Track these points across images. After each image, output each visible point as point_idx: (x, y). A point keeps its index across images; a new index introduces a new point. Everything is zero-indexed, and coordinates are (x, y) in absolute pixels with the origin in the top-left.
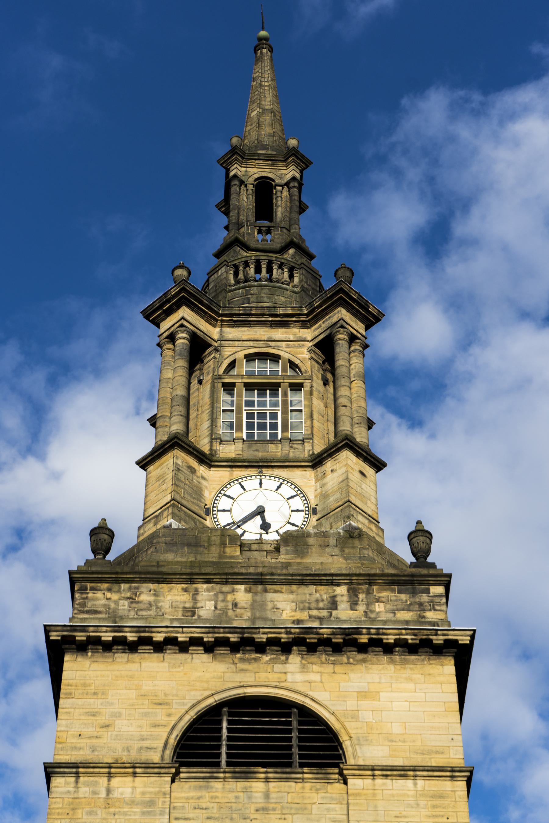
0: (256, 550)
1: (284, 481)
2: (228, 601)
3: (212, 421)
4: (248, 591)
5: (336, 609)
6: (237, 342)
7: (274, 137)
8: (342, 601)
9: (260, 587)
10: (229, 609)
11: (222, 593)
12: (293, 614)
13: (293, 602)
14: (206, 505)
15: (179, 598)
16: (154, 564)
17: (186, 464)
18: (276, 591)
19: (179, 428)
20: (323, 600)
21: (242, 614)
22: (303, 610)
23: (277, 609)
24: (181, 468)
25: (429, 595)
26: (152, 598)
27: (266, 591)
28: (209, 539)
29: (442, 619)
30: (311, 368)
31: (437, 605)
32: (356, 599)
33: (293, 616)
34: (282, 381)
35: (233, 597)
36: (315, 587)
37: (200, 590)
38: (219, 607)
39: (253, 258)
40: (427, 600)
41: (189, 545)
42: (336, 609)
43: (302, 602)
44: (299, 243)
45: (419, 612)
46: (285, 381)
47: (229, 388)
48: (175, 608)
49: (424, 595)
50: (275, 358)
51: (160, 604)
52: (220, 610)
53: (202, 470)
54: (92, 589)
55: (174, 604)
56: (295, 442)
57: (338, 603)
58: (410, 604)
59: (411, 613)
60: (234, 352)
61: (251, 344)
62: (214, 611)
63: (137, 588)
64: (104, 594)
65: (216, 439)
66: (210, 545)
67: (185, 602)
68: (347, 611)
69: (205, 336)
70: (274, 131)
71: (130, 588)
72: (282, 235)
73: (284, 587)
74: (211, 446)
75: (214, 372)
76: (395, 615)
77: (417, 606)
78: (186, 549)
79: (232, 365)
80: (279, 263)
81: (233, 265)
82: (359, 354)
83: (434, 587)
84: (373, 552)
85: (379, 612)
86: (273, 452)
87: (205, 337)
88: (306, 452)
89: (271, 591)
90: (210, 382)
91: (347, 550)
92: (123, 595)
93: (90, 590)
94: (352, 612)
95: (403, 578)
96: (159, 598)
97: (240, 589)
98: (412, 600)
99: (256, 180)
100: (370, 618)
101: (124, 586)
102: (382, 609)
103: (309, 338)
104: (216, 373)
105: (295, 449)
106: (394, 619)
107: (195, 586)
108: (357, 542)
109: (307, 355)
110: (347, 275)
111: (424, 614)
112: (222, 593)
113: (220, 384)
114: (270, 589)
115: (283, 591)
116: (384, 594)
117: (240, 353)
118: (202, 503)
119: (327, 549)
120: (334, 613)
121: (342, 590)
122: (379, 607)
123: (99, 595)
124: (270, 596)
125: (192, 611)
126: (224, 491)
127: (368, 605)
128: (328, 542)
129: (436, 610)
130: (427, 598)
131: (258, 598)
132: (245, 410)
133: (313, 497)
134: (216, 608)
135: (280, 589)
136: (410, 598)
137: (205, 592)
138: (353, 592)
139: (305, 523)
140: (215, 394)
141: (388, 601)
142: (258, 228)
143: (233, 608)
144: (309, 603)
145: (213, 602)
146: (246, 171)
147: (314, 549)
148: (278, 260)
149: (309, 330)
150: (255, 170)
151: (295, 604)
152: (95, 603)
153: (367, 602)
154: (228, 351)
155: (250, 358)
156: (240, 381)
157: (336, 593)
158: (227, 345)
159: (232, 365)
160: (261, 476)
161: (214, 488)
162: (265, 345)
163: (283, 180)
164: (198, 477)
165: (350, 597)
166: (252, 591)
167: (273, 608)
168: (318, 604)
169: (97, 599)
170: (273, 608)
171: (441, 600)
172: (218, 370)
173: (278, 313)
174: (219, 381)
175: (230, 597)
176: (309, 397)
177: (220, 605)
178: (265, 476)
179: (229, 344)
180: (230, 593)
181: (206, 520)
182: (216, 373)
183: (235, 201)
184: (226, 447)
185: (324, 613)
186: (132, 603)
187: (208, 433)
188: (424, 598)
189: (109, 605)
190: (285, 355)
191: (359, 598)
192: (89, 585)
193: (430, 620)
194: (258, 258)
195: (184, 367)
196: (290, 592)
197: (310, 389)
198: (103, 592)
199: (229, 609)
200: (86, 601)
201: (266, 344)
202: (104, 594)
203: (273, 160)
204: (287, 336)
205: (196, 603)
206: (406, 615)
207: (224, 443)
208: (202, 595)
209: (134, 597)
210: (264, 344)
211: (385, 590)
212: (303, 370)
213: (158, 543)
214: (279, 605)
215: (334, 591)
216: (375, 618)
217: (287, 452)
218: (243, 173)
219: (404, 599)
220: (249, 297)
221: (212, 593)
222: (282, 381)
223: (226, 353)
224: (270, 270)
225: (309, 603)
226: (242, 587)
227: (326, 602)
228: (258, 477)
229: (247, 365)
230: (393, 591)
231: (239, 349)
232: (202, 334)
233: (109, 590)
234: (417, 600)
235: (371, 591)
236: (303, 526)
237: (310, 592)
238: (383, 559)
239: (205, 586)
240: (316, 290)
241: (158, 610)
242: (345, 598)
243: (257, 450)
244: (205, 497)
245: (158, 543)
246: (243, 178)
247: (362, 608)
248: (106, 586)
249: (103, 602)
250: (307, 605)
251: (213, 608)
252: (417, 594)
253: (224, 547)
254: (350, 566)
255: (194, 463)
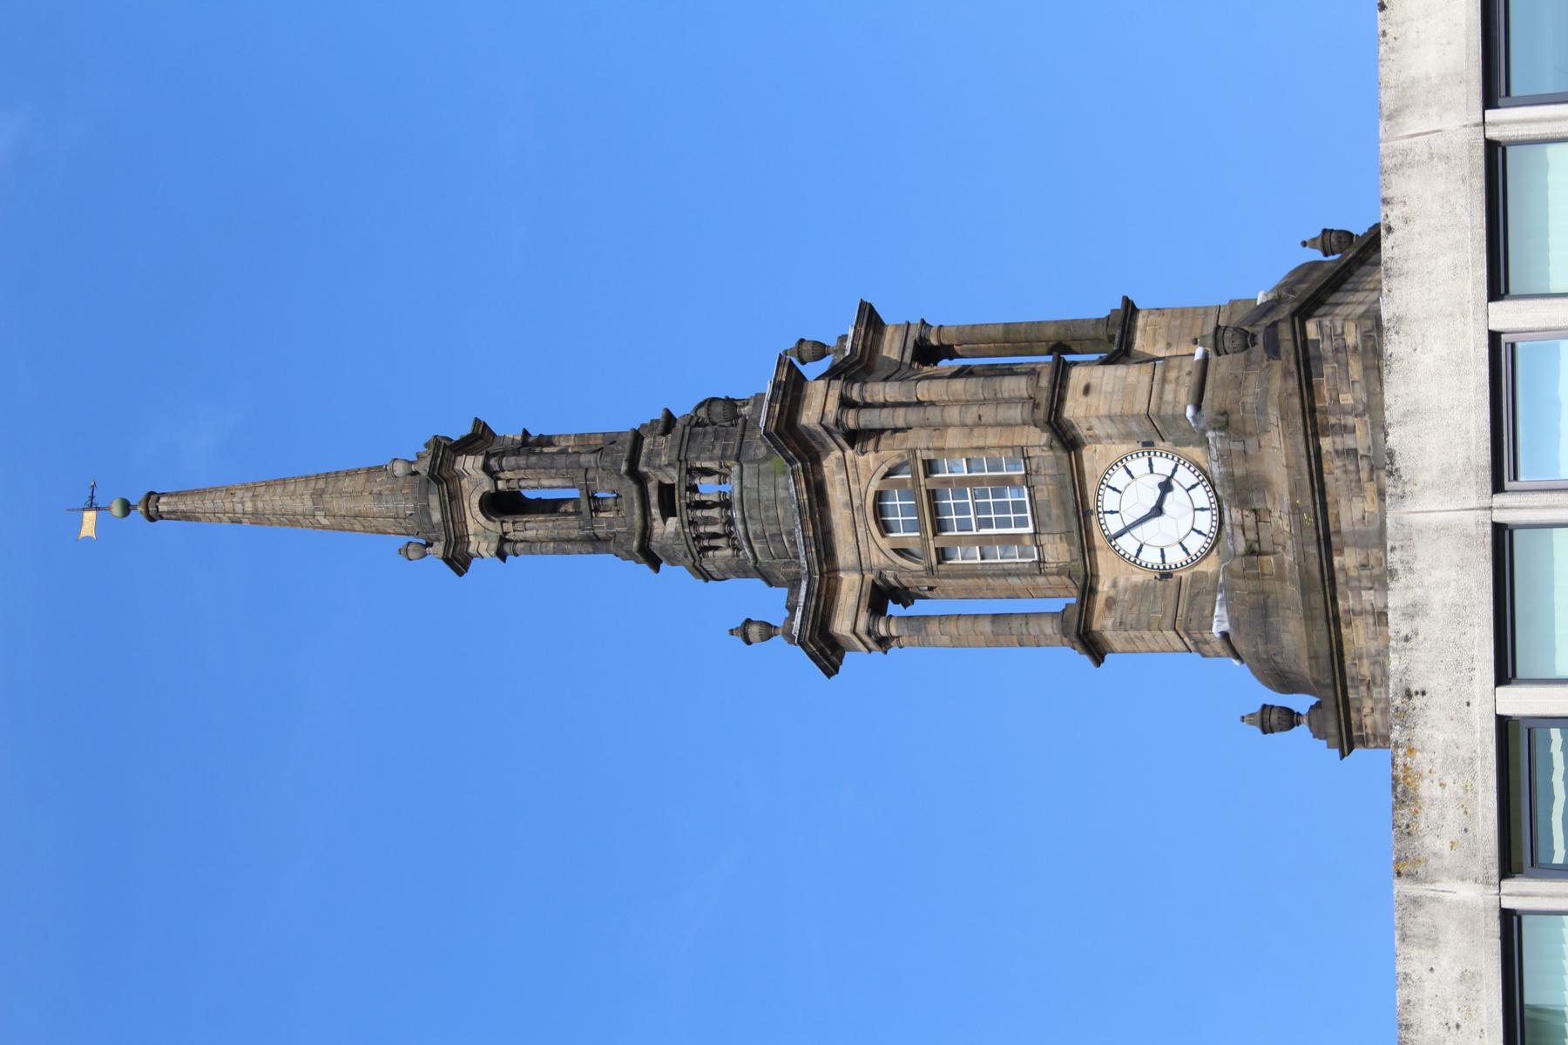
0: (1258, 534)
1: (1102, 483)
2: (1359, 575)
3: (1010, 575)
4: (1341, 553)
5: (1356, 450)
6: (861, 549)
7: (383, 493)
8: (1343, 443)
9: (1334, 539)
10: (1371, 574)
11: (1347, 583)
12: (1369, 499)
13: (1351, 500)
14: (1156, 578)
15: (1361, 632)
16: (1313, 661)
17: (1107, 613)
18: (1338, 520)
19: (1050, 625)
20: (1345, 465)
21: (1377, 558)
22: (1361, 489)
23: (1364, 518)
24: (1118, 620)
25: (1320, 339)
26: (1366, 662)
27: (1338, 532)
28: (1254, 593)
29: (1356, 326)
30: (893, 450)
31: (1335, 331)
32: (1337, 427)
33: (1373, 500)
34: (923, 488)
35: (1352, 569)
36: (1325, 475)
37: (1347, 607)
38: (1370, 585)
39: (687, 530)
40: (1329, 343)
41: (1266, 616)
42: (1356, 450)
43: (1349, 489)
44: (626, 460)
45: (1349, 353)
46: (922, 482)
47: (942, 555)
48: (1376, 634)
49: (1321, 346)
50: (879, 496)
51: (1374, 652)
52: (1373, 583)
53: (1104, 587)
54: (1360, 728)
55: (1371, 636)
56: (1028, 468)
57: (1346, 447)
58: (1338, 362)
59: (1351, 362)
60: (878, 551)
61: (861, 530)
62: (1375, 590)
63: (1353, 679)
64: (1365, 716)
65: (1040, 569)
66: (1263, 592)
67: (1367, 624)
68: (1358, 438)
69: (863, 594)
70: (367, 494)
71: (1354, 687)
72: (602, 480)
73: (1330, 510)
74: (1052, 574)
75: (922, 577)
76: (1357, 382)
77: (1340, 355)
78: (1272, 620)
79: (902, 552)
80: (688, 493)
81: (699, 553)
82: (866, 392)
83: (1308, 334)
84: (1243, 395)
85: (1354, 400)
86: (1049, 495)
87: (866, 594)
88: (1046, 454)
89: (1337, 525)
90: (938, 580)
91: (1249, 429)
92: (1365, 694)
93: (1362, 731)
94: (1357, 432)
95: (1302, 373)
96: (1365, 654)
97: (1339, 562)
98: (1330, 361)
99: (488, 519)
100: (1364, 411)
101: (1351, 694)
102: (1349, 396)
103: (838, 453)
104: (923, 574)
105: (1038, 468)
106: (1363, 382)
107: (1341, 615)
108: (1234, 417)
109: (871, 456)
110: (722, 411)
111: (1351, 347)
112: (1347, 583)
113: (940, 567)
114: (1335, 527)
115: (1336, 512)
116: (1326, 393)
117: (880, 544)
118: (1156, 585)
119: (1251, 452)
120: (1361, 452)
121: (1326, 443)
122: (1347, 399)
123: (1368, 721)
124: (1344, 526)
125: (1378, 616)
126: (1158, 567)
127: (1346, 413)
128: (1240, 451)
129: (1343, 333)
130: (1325, 343)
131: (1350, 541)
132: (977, 531)
133: (1125, 446)
134: (1370, 589)
135: (1334, 516)
136: (1327, 363)
137: (1349, 602)
138: (1328, 430)
139: (1170, 457)
140: (961, 572)
141: (1336, 391)
142: (594, 514)
143: (1369, 569)
144: (1351, 482)
145: (1363, 592)
146: (475, 535)
147: (1253, 468)
148: (683, 495)
149: (821, 453)
150: (470, 522)
151: (1354, 498)
152: (1380, 725)
153: (1340, 413)
154: (877, 559)
155: (885, 528)
156: (931, 542)
157: (1331, 450)
158: (868, 561)
159: (902, 552)
160: (1099, 513)
161: (1127, 569)
162: (861, 512)
163: (482, 479)
164: (1117, 593)
165: (1336, 434)
166: (1340, 548)
167: (1364, 523)
168: (1350, 471)
169: (1375, 723)
170: (1364, 523)
171: (1327, 326)
172: (915, 571)
173: (807, 501)
174: (935, 569)
175: (1353, 573)
176: (946, 452)
177: (1366, 583)
178: (1098, 507)
179: (865, 558)
180: (1346, 574)
181: (1181, 578)
182: (923, 574)
183: (548, 549)
184: (1048, 554)
185: (1363, 464)
186: (1374, 684)
187: (1029, 579)
188: (1326, 346)
189: (1382, 709)
190: (875, 485)
191: (1336, 424)
192: (1355, 733)
193: (1359, 339)
194: (686, 524)
195: (940, 623)
196: (1335, 505)
197: (932, 451)
198: (1363, 717)
199: (1371, 574)
200: (1378, 735)
201: (858, 509)
202: (1365, 716)
203: (453, 499)
204: (837, 483)
205: (1367, 612)
206: (1354, 368)
207: (1042, 557)
208: (1353, 605)
209: (1366, 682)
210: (858, 514)
211: (1319, 392)
212: (898, 461)
213: (1267, 652)
214: (1359, 516)
215: (1328, 452)
216: (1364, 404)
217: (1047, 478)
218: (481, 539)
219: (1330, 370)
220: (770, 535)
221: (1350, 594)
222: (923, 488)
223: (882, 561)
224: (702, 505)
225: (1351, 482)
226: (1337, 560)
227: (1347, 463)
228: (1101, 516)
229: (895, 530)
230: (1320, 384)
231: (872, 546)
232: (862, 599)
233: (1359, 710)
234: (1330, 354)
235: (1324, 409)
236: (1176, 459)
237: (1334, 481)
238: (1245, 378)
239: (1340, 602)
240: (715, 431)
241: (1381, 653)
242: (1338, 439)
243: (1049, 515)
244: (1144, 581)
245: (1267, 652)
246: (496, 539)
247: (1350, 420)
248: (1353, 715)
249: (1377, 716)
250: (1353, 484)
251: (1372, 592)
252: (1321, 355)
253: (1263, 575)
254: (1287, 435)
255: (1100, 601)
